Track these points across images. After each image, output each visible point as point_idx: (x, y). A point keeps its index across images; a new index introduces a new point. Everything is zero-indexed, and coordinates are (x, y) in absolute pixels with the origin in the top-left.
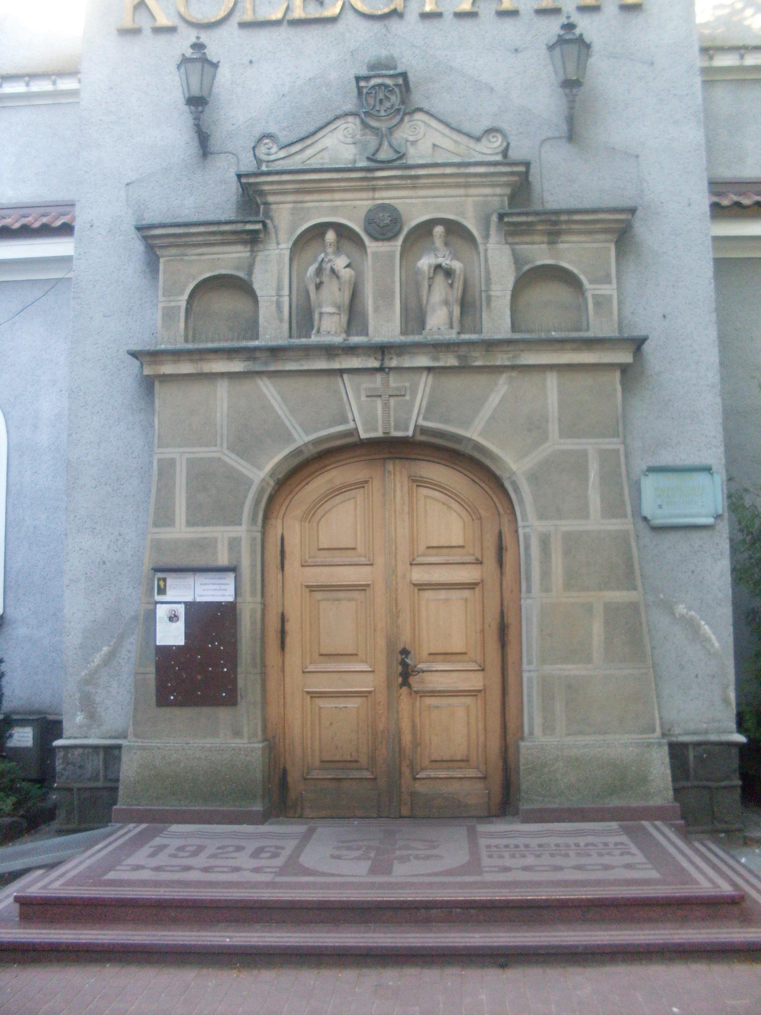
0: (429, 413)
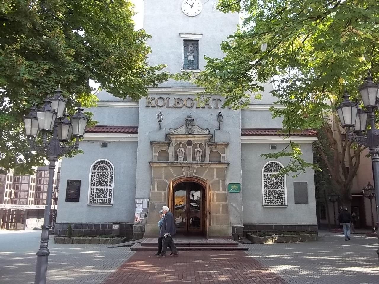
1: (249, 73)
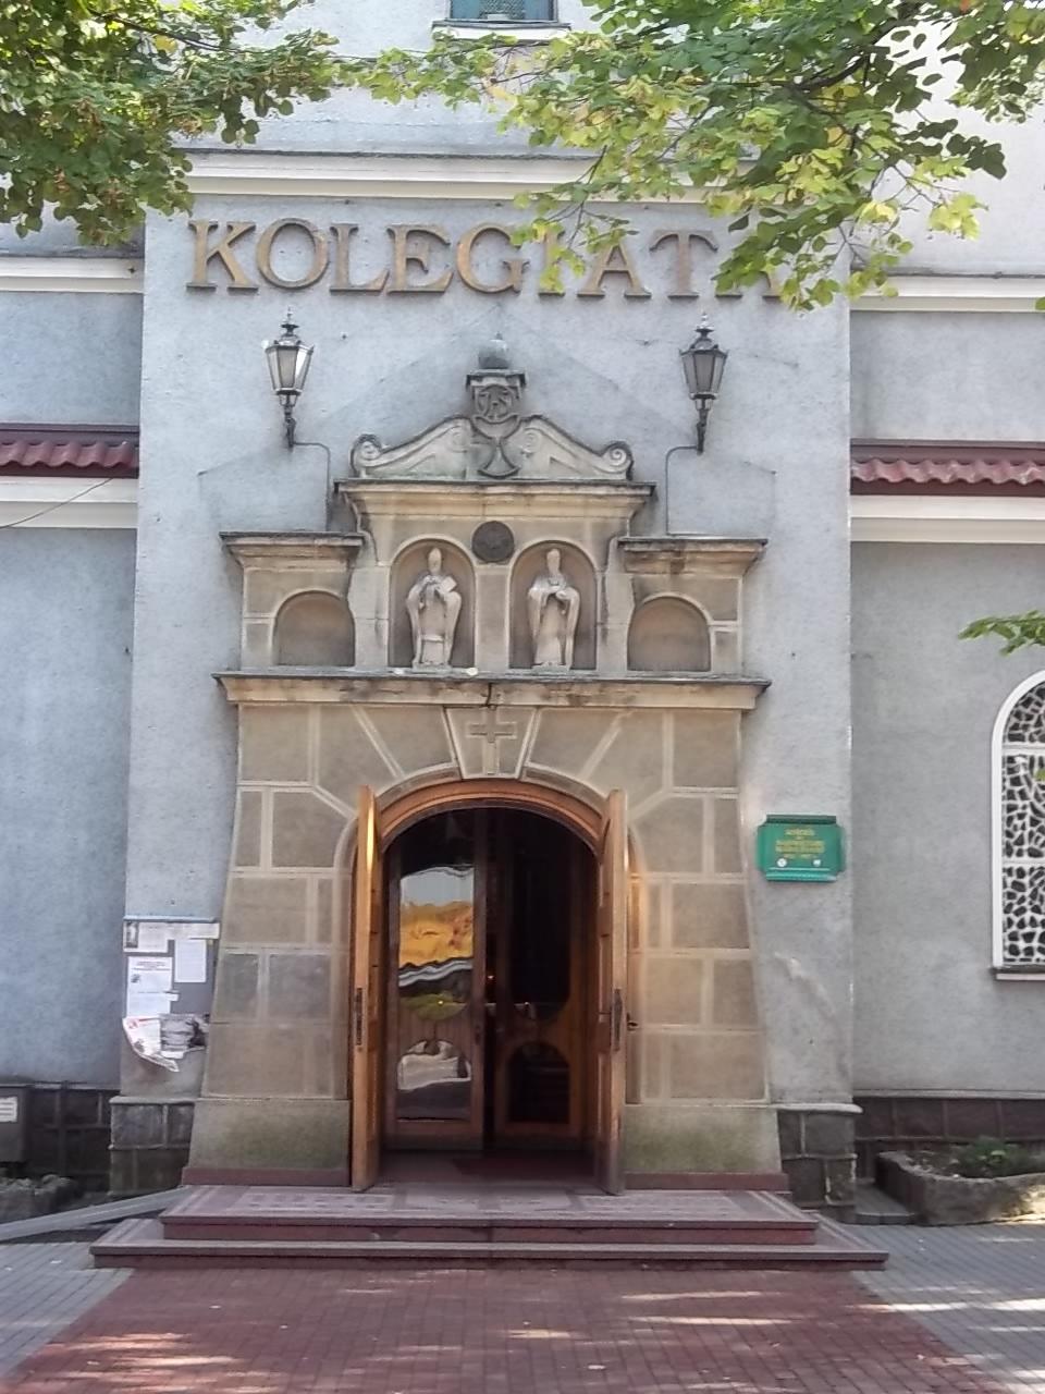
0: (538, 753)
1: (897, 49)
